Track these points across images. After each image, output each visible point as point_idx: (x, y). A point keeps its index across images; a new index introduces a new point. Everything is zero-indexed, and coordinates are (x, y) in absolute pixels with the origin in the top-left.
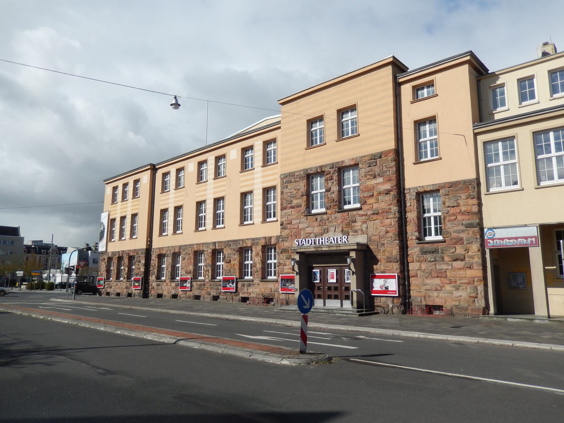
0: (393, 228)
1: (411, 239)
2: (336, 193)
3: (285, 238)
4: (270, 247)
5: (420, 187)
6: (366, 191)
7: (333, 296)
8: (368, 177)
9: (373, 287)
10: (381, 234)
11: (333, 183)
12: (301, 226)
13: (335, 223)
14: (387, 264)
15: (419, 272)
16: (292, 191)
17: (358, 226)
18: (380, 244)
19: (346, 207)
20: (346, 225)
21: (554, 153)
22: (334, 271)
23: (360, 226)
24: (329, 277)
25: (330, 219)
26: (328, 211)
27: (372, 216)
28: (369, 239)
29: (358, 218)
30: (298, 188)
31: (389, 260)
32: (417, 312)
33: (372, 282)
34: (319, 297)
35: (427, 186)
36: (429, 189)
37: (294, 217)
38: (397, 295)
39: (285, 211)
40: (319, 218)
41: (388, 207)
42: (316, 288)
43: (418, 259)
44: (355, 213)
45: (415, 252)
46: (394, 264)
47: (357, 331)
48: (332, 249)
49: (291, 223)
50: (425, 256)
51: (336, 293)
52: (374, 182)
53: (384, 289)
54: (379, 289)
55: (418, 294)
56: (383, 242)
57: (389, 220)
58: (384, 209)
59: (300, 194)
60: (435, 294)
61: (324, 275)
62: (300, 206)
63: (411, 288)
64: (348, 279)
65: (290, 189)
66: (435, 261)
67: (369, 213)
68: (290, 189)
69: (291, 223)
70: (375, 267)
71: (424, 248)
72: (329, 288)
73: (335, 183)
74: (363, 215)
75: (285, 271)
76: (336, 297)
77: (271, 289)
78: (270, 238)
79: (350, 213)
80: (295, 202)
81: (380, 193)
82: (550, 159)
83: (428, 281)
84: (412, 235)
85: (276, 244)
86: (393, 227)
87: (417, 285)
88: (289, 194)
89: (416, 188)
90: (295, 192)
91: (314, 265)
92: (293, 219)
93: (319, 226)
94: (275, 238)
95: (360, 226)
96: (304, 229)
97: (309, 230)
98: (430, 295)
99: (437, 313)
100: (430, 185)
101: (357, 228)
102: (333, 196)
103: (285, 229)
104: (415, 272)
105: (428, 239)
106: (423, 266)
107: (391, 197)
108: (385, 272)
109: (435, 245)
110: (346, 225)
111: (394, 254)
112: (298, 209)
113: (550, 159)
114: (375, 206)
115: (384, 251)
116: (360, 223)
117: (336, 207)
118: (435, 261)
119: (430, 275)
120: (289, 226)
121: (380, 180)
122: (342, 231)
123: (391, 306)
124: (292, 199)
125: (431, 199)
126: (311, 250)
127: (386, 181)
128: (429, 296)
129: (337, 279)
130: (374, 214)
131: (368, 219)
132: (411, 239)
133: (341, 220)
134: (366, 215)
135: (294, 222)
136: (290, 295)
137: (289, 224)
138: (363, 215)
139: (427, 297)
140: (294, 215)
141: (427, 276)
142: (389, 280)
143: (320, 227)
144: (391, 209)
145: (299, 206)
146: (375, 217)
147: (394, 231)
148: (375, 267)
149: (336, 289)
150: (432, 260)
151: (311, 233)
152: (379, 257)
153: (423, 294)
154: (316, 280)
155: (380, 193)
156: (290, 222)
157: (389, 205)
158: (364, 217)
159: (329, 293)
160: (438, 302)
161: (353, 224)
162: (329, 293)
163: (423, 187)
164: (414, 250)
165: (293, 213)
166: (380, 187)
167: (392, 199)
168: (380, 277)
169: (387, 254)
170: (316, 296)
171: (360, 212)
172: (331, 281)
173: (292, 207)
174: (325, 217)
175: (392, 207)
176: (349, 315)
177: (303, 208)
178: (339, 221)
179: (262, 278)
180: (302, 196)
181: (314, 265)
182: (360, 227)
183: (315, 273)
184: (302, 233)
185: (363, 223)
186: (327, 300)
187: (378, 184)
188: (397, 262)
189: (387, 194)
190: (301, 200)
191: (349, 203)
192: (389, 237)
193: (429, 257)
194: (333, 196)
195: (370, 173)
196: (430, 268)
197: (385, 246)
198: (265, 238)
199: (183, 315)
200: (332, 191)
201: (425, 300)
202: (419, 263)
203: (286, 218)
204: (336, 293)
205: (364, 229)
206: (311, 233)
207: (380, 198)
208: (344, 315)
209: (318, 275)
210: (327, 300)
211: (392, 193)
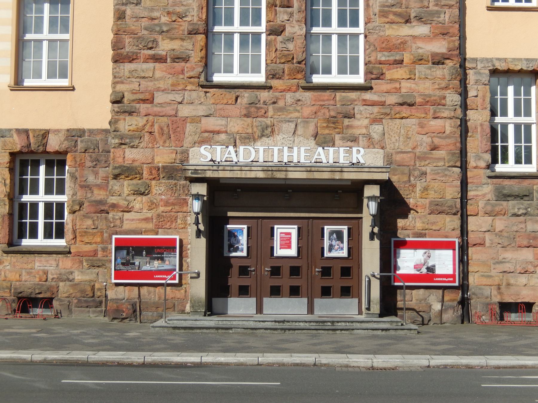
0: (449, 141)
1: (476, 168)
2: (300, 42)
3: (132, 137)
4: (30, 157)
5: (499, 59)
6: (382, 50)
7: (286, 290)
8: (391, 17)
9: (396, 268)
10: (417, 150)
11: (291, 14)
12: (185, 111)
13: (297, 114)
14: (433, 217)
15: (488, 237)
16: (156, 14)
17: (358, 127)
18: (416, 173)
19: (318, 79)
20: (328, 121)
21: (334, 28)
22: (293, 230)
23: (366, 127)
24: (277, 243)
25: (281, 104)
26: (274, 83)
27: (398, 108)
28: (389, 161)
29: (359, 108)
30: (179, 9)
31: (437, 209)
32: (479, 317)
33: (396, 256)
34: (244, 291)
35: (514, 59)
36: (518, 68)
37: (162, 85)
38: (457, 284)
39: (128, 67)
40: (246, 96)
41: (438, 93)
42: (235, 271)
43: (489, 208)
44: (353, 95)
45: (484, 195)
46: (448, 218)
47: (521, 367)
48: (317, 176)
49: (150, 101)
50: (505, 203)
51: (295, 282)
52: (405, 31)
53: (424, 271)
54: (413, 272)
55: (485, 281)
56: (424, 169)
57: (439, 122)
58: (430, 96)
59: (185, 27)
60: (523, 279)
61: (261, 238)
62: (186, 59)
63: (471, 269)
64: (331, 248)
65: (152, 10)
66: (525, 214)
67: (392, 99)
68: (152, 10)
69: (150, 101)
70: (401, 223)
71: (504, 188)
72: (276, 271)
73: (296, 16)
74: (373, 104)
75: (126, 226)
76: (295, 292)
77: (46, 273)
78: (45, 134)
79: (339, 95)
80: (165, 46)
81: (420, 60)
82: (328, 37)
83: (509, 255)
84: (478, 158)
85: (66, 153)
86: (448, 137)
87: (484, 263)
88: (145, 23)
89: (491, 60)
90: (164, 19)
91: (230, 214)
92: (158, 90)
93: (247, 116)
94: (62, 136)
95: (366, 127)
96: (196, 120)
97: (212, 123)
98: (512, 281)
99: (513, 317)
100: (520, 60)
101: (357, 132)
102: (291, 46)
103: (131, 113)
104: (481, 235)
105: (500, 168)
106: (500, 224)
107: (446, 72)
108: (424, 235)
109: (526, 183)
110: (328, 121)
111: (448, 196)
112: (179, 66)
113: (328, 37)
114: (406, 86)
115: (426, 189)
116: (366, 122)
117: (300, 76)
118: (525, 214)
119: (511, 242)
120: (143, 108)
121: (422, 30)
122: (316, 136)
123: (437, 307)
124: (159, 38)
125: (511, 89)
126: (252, 175)
127: (436, 35)
128: (508, 285)
129: (299, 249)
130: (401, 104)
131: (385, 113)
132: (476, 168)
133: (314, 109)
134: (382, 104)
135: (159, 98)
136: (144, 290)
137: (144, 101)
138: (373, 104)
139: (503, 287)
140: (161, 78)
141: (506, 244)
142: (438, 252)
143: (249, 120)
144: (444, 98)
145: (180, 58)
146: (405, 111)
147: (452, 147)
148: (401, 223)
149: (295, 271)
150: (521, 212)
151: (218, 132)
152: (411, 202)
153: (497, 281)
154: (236, 250)
155: (420, 60)
156: (147, 96)
157: (442, 89)
158: (376, 109)
159: (276, 282)
160: (525, 296)
161: (346, 122)
162: (276, 282)
163: (505, 60)
164: (482, 192)
165: (158, 74)
166: (420, 44)
167: (448, 77)
168: (415, 246)
169: (432, 195)
170: (234, 289)
171: (368, 96)
172: (279, 252)
173: (158, 59)
174: (264, 95)
175: (447, 93)
176: (392, 333)
177: (194, 66)
178: (307, 111)
179: (10, 244)
180: (193, 33)
181: (230, 214)
182: (364, 131)
183: (232, 234)
184: (189, 128)
185: (375, 121)
186: (266, 300)
187: (414, 37)
188: (455, 214)
189: (438, 63)
190: (187, 44)
191: (327, 71)
192: (439, 159)
193: (512, 205)
194: (291, 46)
195: (394, 9)
196: (515, 228)
197: (429, 177)
198: (26, 131)
199: (221, 364)
200: (287, 33)
201: (500, 293)
202: (491, 218)
203: (135, 86)
204: (295, 282)
205: (376, 137)
206: (218, 132)
207: (421, 69)
208: (379, 333)
209: (243, 239)
210: (266, 300)
211: (449, 63)
